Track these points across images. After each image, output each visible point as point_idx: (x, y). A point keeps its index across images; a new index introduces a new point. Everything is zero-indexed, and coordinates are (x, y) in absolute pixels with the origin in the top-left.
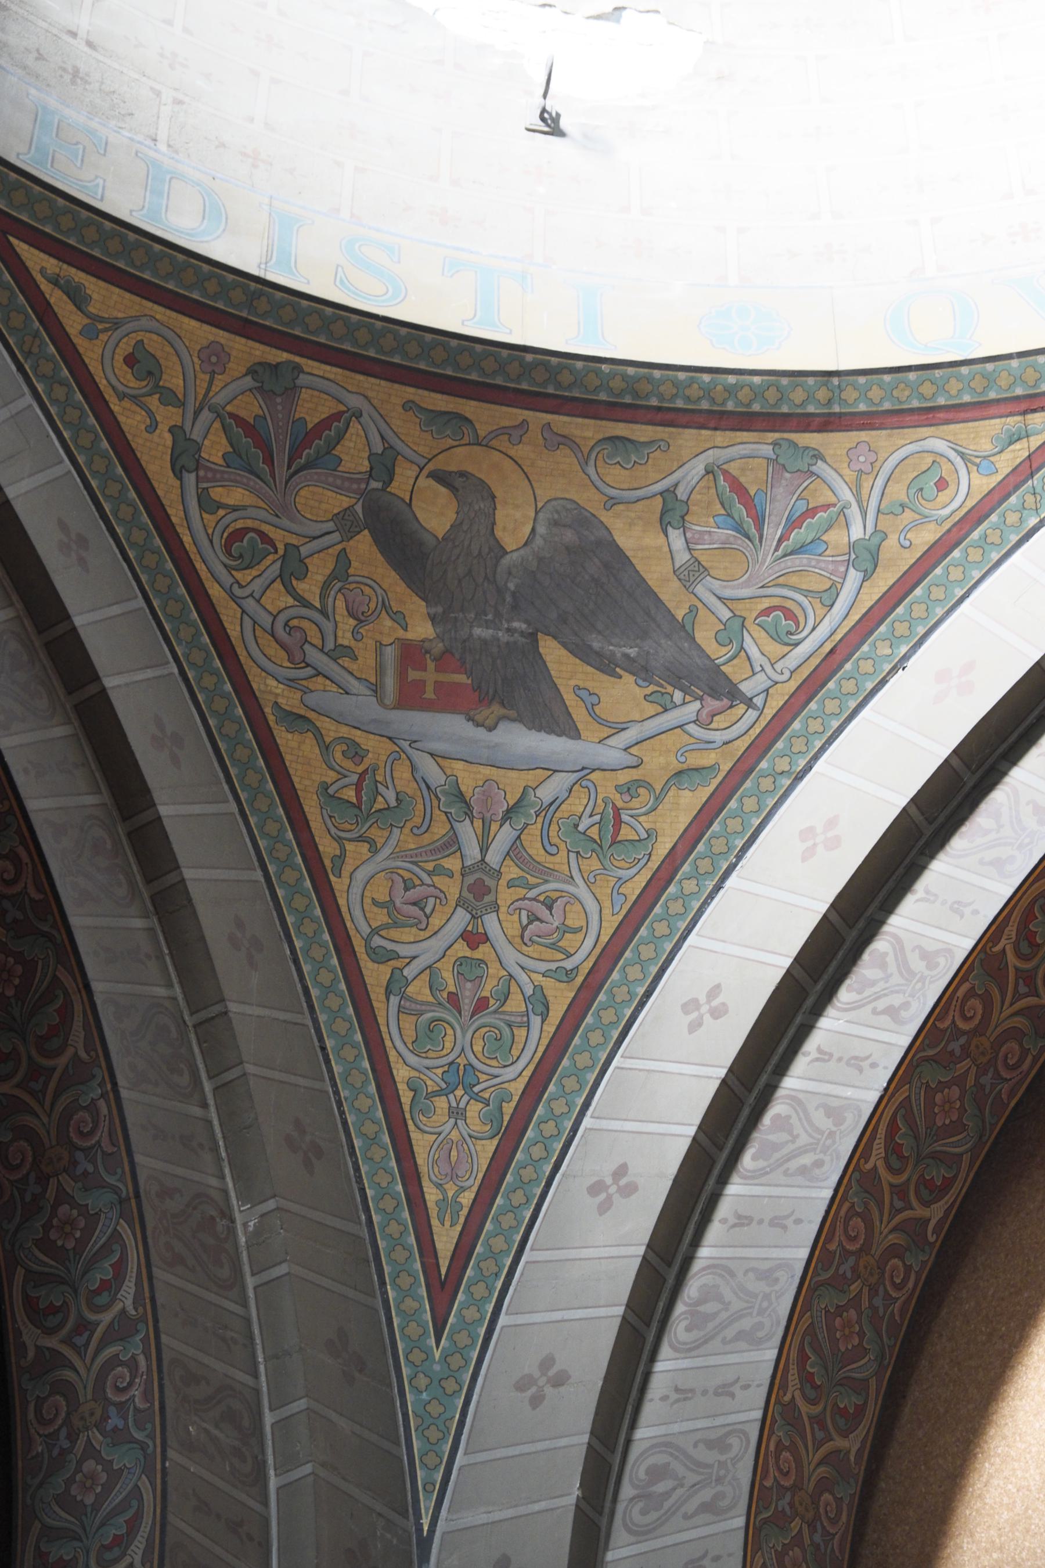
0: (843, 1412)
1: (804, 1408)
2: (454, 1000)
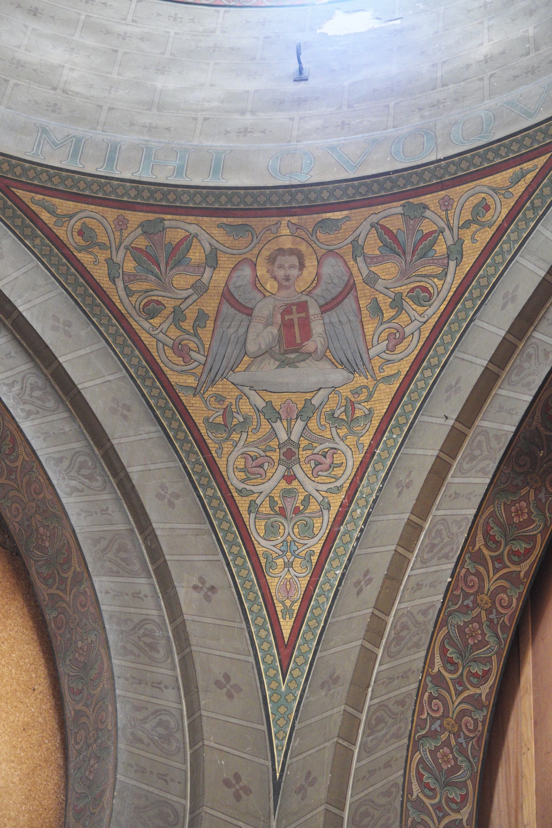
2: (282, 512)
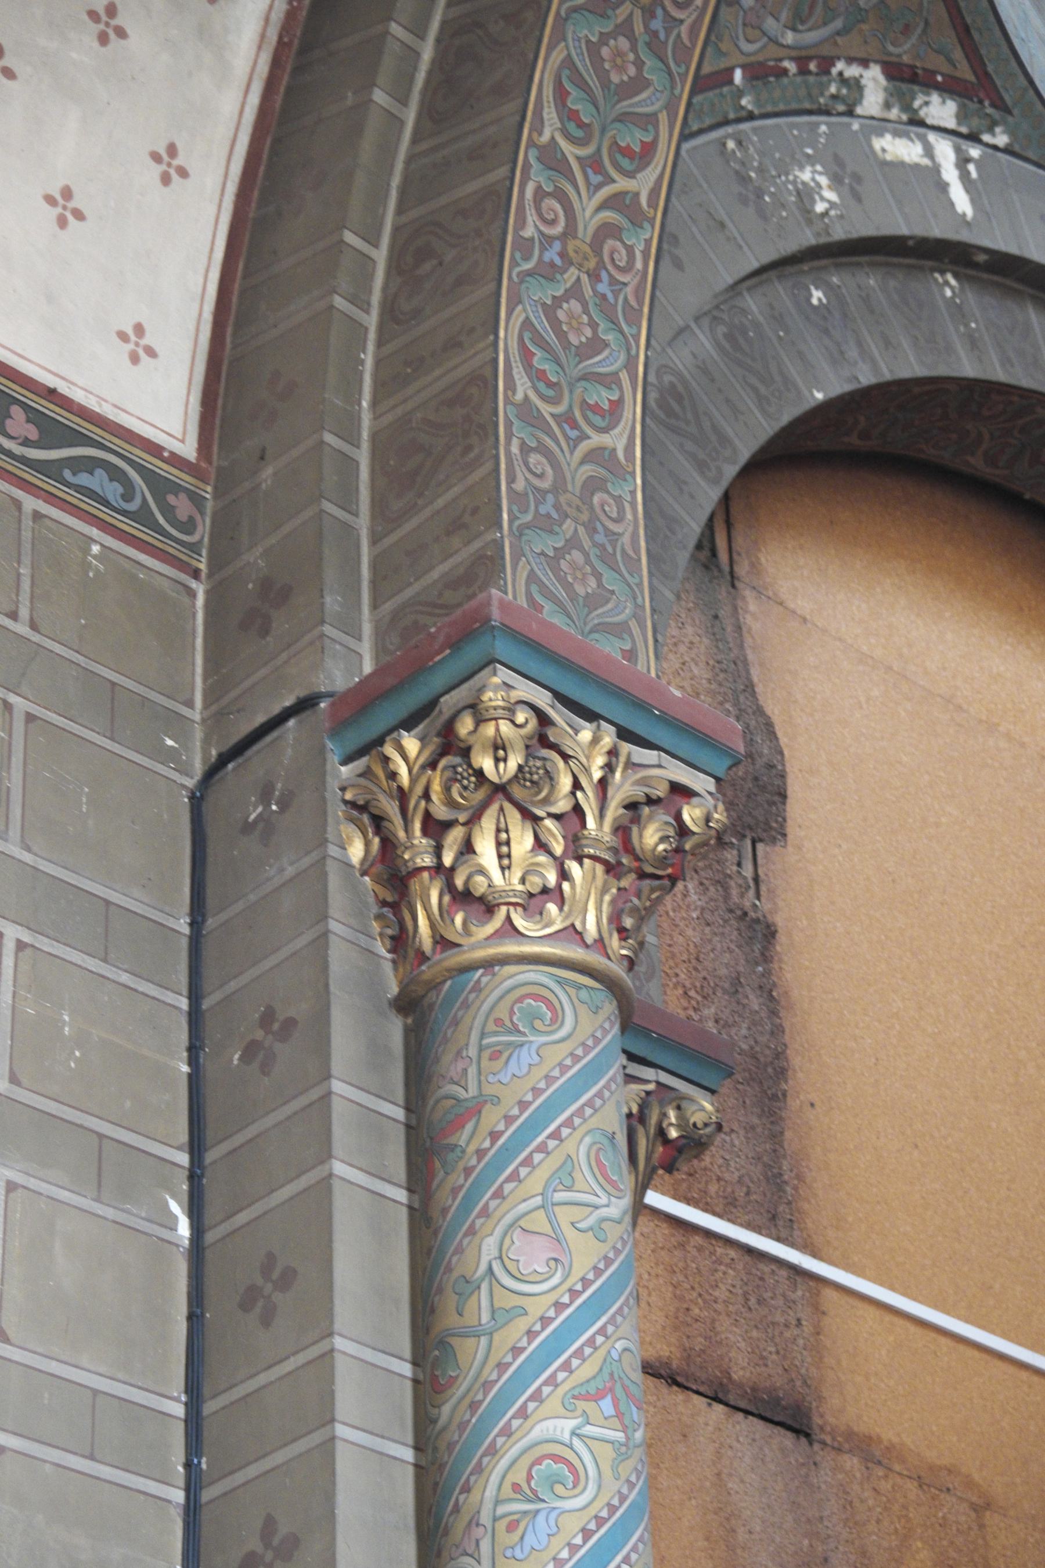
0: (596, 409)
1: (546, 409)
